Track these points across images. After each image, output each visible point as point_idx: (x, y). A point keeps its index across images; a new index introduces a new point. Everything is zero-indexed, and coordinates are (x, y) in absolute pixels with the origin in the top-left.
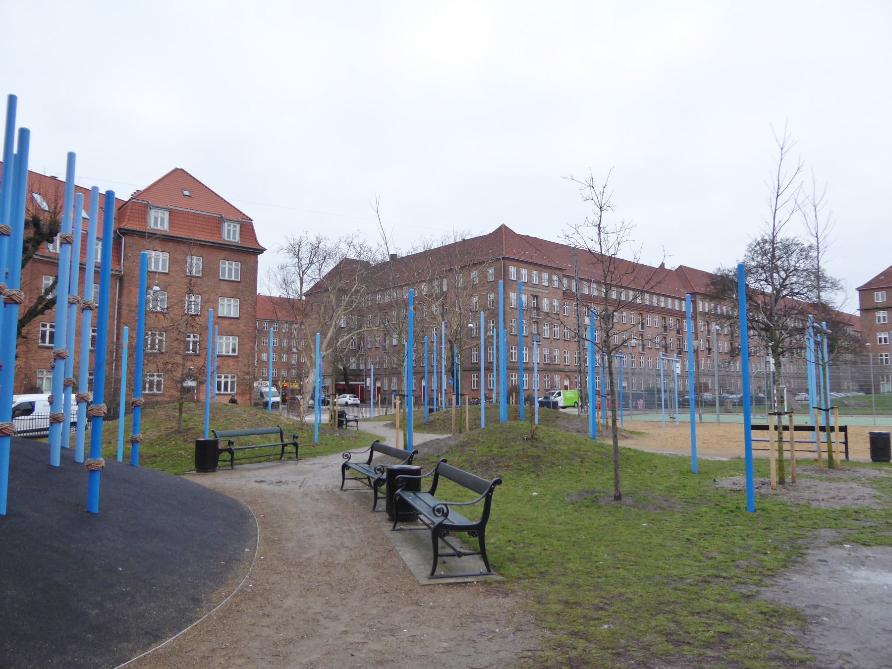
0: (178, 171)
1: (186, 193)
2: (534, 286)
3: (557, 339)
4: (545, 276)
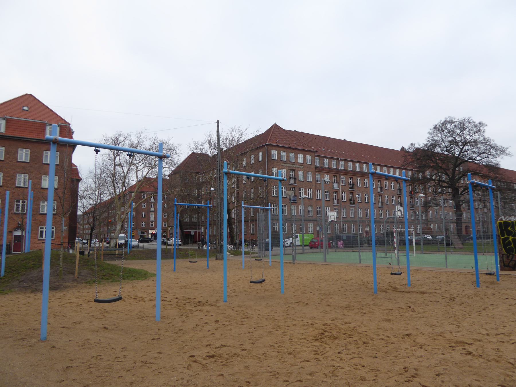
0: (31, 96)
1: (25, 108)
2: (292, 163)
3: (311, 199)
4: (309, 157)
